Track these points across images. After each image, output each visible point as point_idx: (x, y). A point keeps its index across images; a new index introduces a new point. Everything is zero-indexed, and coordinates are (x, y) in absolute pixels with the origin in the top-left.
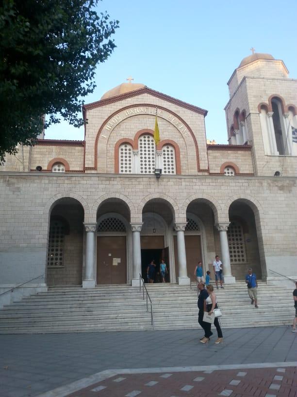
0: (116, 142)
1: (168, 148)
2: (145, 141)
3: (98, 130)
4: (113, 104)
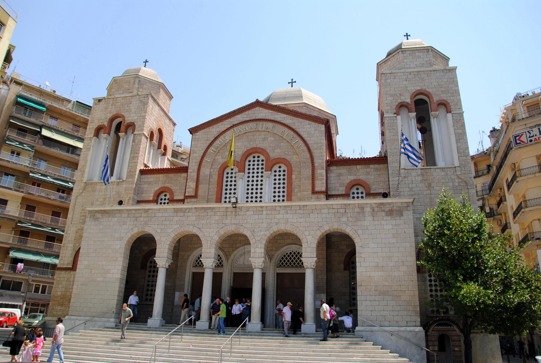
0: (220, 166)
4: (220, 124)
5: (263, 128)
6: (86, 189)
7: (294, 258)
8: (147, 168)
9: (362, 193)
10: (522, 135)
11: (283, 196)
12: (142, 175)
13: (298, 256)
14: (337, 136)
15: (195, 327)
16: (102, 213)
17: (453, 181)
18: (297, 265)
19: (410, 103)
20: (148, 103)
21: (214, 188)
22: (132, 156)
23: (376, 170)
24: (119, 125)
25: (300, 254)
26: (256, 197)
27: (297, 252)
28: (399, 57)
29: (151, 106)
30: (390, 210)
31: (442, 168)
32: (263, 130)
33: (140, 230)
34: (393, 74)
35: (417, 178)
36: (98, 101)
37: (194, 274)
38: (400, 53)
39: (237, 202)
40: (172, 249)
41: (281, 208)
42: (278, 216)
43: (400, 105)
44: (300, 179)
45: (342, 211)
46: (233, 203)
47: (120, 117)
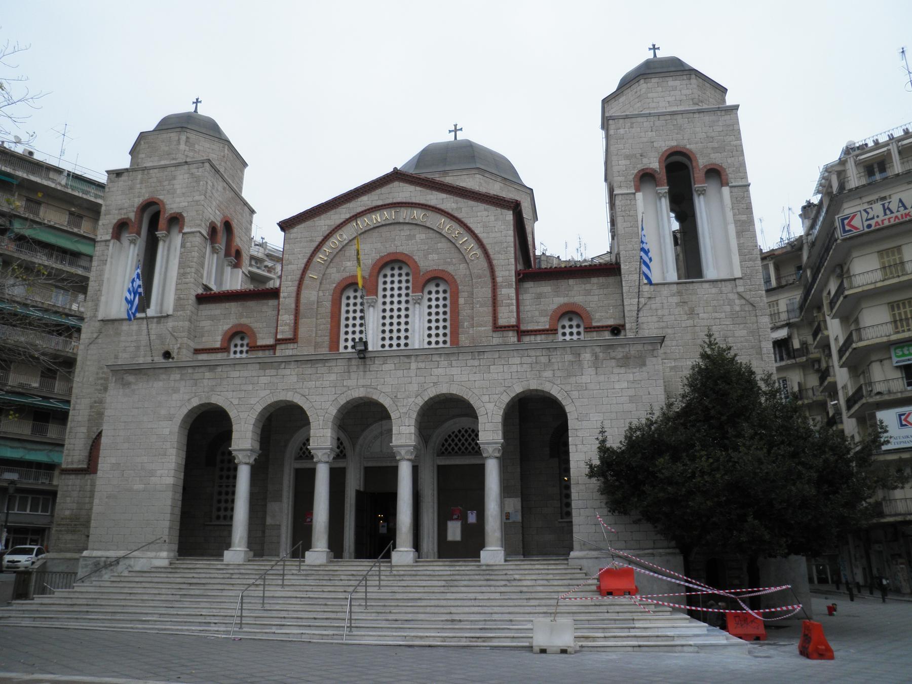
0: (334, 285)
1: (437, 285)
2: (393, 275)
4: (332, 212)
9: (578, 326)
10: (854, 216)
13: (473, 435)
15: (304, 561)
17: (731, 303)
18: (472, 451)
19: (659, 170)
22: (182, 271)
25: (475, 433)
27: (470, 428)
35: (670, 299)
36: (115, 175)
40: (259, 431)
41: (440, 357)
42: (436, 371)
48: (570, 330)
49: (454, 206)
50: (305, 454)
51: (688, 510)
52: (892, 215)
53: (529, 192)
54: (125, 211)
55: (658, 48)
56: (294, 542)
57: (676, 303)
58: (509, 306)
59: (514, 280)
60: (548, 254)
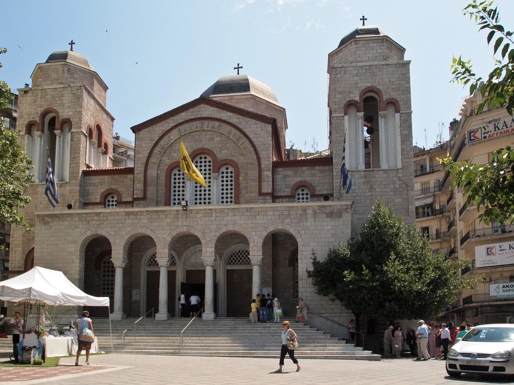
0: (167, 167)
3: (148, 154)
4: (164, 122)
5: (209, 128)
6: (26, 191)
7: (241, 259)
8: (90, 169)
9: (307, 194)
10: (477, 131)
11: (231, 198)
12: (85, 176)
13: (246, 254)
14: (287, 130)
15: (155, 319)
16: (51, 217)
17: (394, 183)
18: (246, 262)
19: (359, 102)
20: (82, 96)
21: (162, 190)
22: (72, 156)
23: (322, 171)
24: (52, 121)
25: (248, 253)
26: (205, 199)
27: (245, 250)
28: (351, 48)
29: (86, 100)
30: (330, 212)
31: (385, 170)
32: (209, 129)
33: (93, 233)
34: (344, 68)
35: (360, 180)
36: (23, 92)
37: (148, 272)
38: (353, 43)
39: (187, 205)
40: (127, 250)
41: (229, 211)
42: (226, 218)
43: (348, 103)
44: (247, 181)
45: (286, 213)
46: (183, 206)
47: (52, 112)
48: (302, 196)
49: (237, 120)
50: (153, 261)
51: (331, 277)
52: (499, 131)
53: (283, 110)
54: (32, 116)
55: (366, 19)
56: (147, 310)
57: (363, 182)
58: (268, 182)
59: (271, 167)
60: (294, 148)
